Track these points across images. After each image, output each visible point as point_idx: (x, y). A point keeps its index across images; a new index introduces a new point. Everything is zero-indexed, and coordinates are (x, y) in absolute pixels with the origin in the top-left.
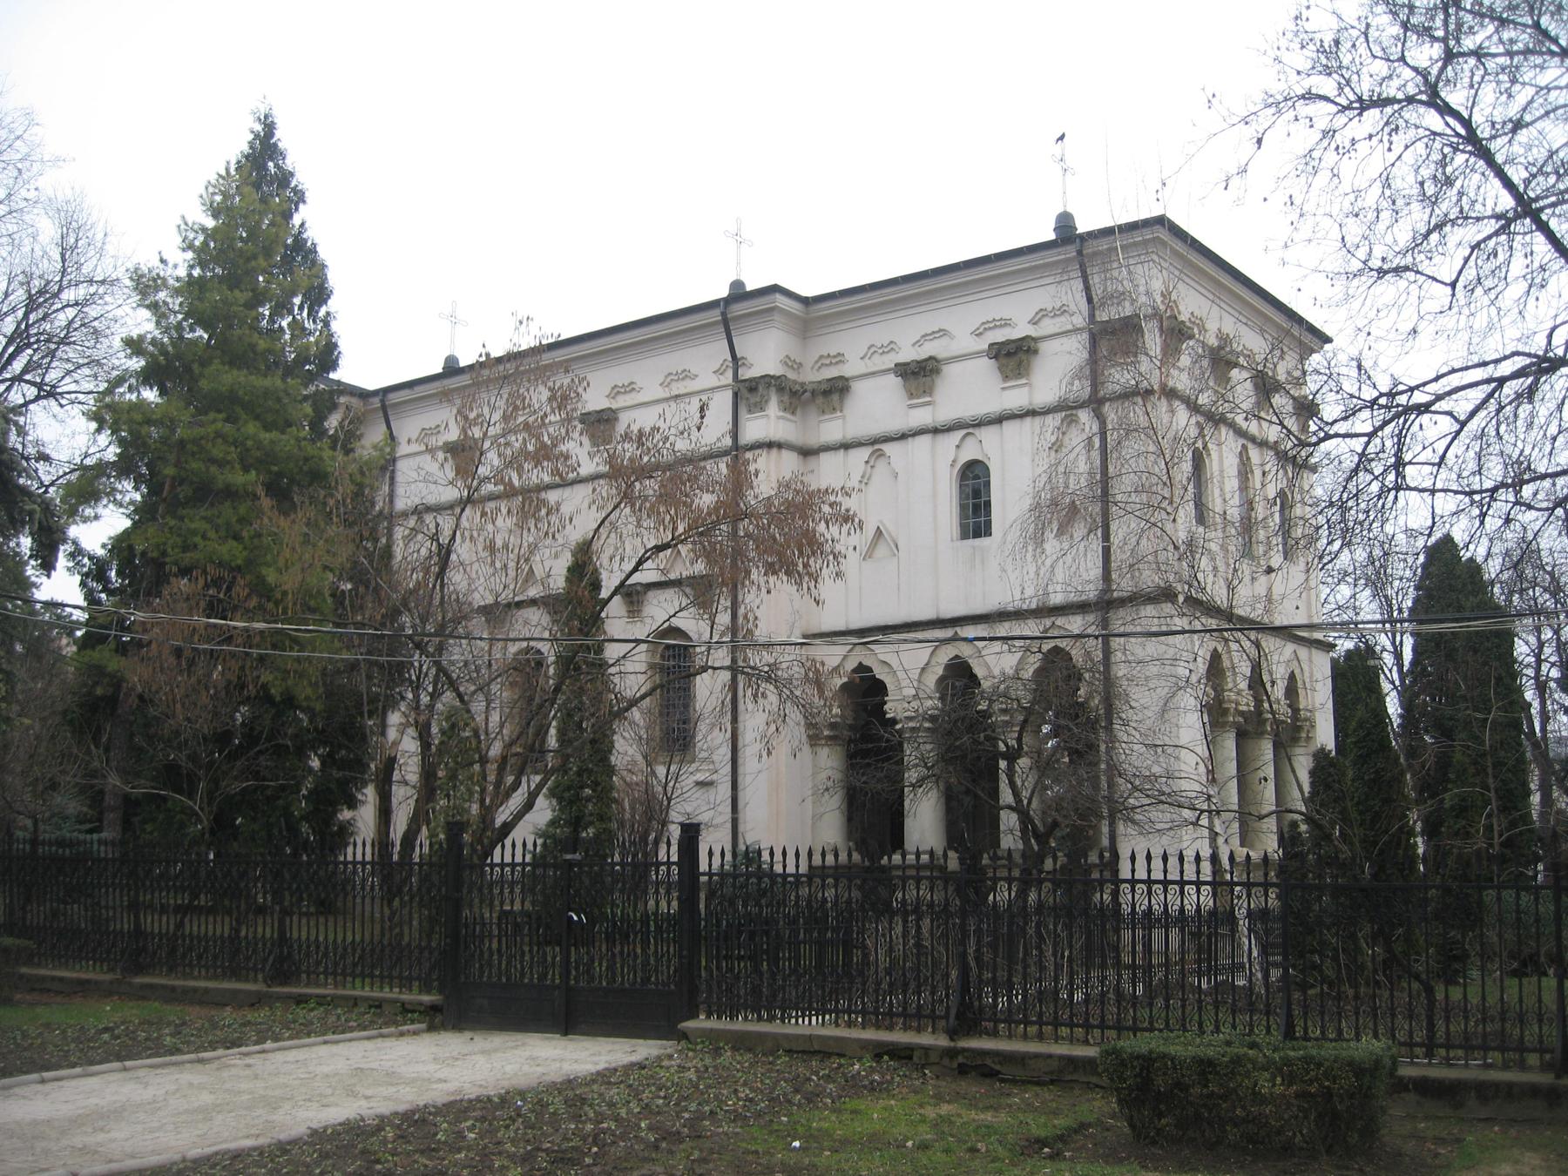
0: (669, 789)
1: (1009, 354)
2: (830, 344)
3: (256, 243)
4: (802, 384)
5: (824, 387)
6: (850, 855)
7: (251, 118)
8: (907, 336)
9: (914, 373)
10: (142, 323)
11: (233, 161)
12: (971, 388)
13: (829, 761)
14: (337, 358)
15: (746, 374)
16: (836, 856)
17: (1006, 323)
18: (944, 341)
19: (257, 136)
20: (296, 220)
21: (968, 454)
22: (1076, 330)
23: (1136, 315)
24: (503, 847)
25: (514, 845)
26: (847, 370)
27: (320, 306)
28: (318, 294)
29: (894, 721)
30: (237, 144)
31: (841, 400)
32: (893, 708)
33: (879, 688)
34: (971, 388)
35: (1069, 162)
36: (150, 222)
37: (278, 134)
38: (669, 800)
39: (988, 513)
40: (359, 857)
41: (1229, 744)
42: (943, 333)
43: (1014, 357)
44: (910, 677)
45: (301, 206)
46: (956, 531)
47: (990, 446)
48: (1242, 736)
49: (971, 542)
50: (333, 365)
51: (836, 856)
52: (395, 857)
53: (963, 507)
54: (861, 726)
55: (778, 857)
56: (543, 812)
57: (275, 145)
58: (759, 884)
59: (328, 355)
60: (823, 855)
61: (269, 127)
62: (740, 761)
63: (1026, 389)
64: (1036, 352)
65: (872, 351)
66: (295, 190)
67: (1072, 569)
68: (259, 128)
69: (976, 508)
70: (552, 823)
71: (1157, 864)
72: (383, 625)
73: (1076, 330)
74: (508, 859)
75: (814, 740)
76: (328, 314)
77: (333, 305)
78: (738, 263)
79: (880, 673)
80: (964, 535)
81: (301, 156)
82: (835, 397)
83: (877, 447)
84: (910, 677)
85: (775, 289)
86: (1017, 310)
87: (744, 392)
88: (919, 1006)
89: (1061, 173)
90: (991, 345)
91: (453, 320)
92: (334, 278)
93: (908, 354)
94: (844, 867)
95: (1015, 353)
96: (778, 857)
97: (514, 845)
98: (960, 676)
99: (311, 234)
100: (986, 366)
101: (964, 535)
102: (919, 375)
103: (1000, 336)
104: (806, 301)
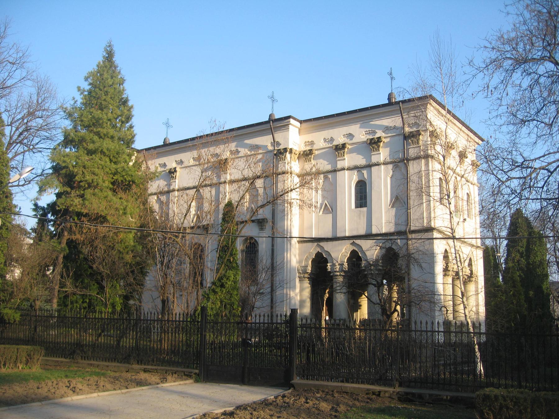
3: (105, 101)
6: (311, 320)
10: (67, 124)
11: (101, 61)
16: (307, 320)
30: (99, 57)
33: (359, 259)
35: (389, 77)
36: (69, 89)
40: (177, 319)
48: (465, 283)
49: (359, 209)
50: (133, 142)
51: (307, 320)
58: (264, 326)
60: (302, 320)
61: (109, 56)
71: (262, 318)
72: (52, 289)
78: (273, 108)
80: (357, 207)
83: (325, 174)
94: (304, 324)
98: (355, 258)
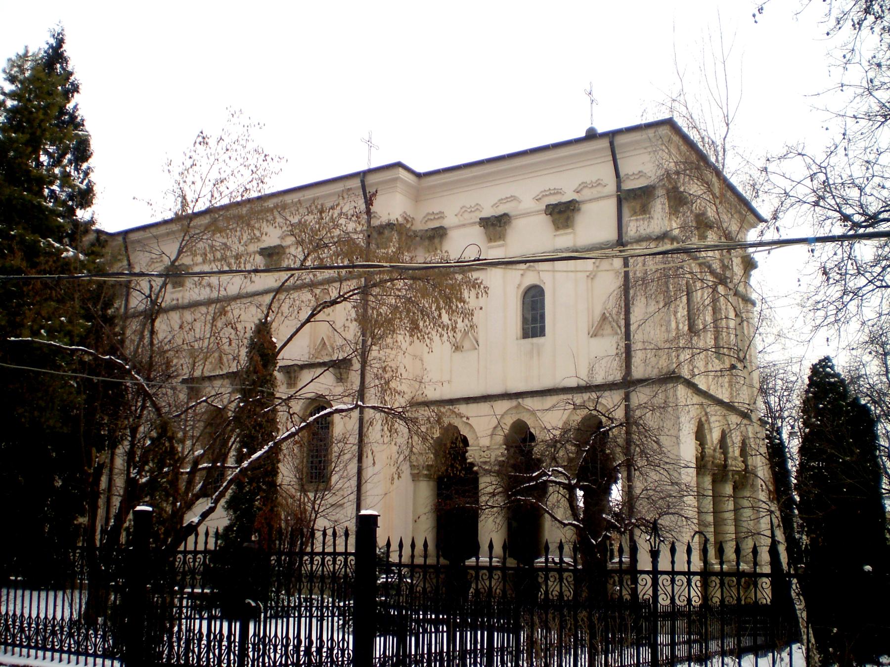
0: (316, 507)
1: (560, 212)
2: (434, 206)
4: (415, 232)
5: (429, 234)
7: (49, 34)
8: (488, 200)
9: (493, 225)
12: (531, 235)
13: (426, 492)
14: (92, 198)
15: (375, 222)
17: (558, 192)
18: (514, 204)
19: (51, 47)
20: (70, 106)
21: (531, 279)
22: (608, 197)
23: (676, 205)
24: (197, 535)
25: (207, 534)
26: (446, 223)
27: (83, 162)
28: (82, 152)
29: (472, 465)
31: (441, 243)
32: (473, 455)
34: (531, 235)
37: (65, 47)
38: (317, 513)
39: (544, 322)
41: (707, 481)
42: (513, 198)
43: (563, 213)
44: (485, 435)
45: (75, 94)
46: (519, 332)
47: (542, 275)
49: (530, 340)
52: (150, 509)
53: (525, 320)
54: (451, 475)
55: (394, 546)
56: (221, 519)
57: (62, 53)
59: (85, 197)
61: (60, 42)
62: (362, 498)
63: (572, 235)
64: (579, 210)
65: (464, 210)
66: (72, 84)
67: (598, 358)
68: (53, 42)
69: (534, 320)
70: (227, 529)
73: (608, 197)
74: (200, 547)
75: (415, 477)
76: (89, 168)
77: (91, 162)
79: (464, 431)
80: (526, 335)
81: (79, 62)
82: (437, 241)
84: (485, 435)
85: (399, 165)
86: (565, 184)
87: (375, 235)
88: (490, 578)
89: (593, 93)
90: (548, 206)
91: (756, 22)
92: (95, 145)
93: (488, 212)
95: (564, 211)
96: (394, 546)
97: (207, 534)
99: (81, 113)
100: (544, 220)
101: (526, 335)
102: (496, 225)
103: (554, 200)
104: (419, 175)
